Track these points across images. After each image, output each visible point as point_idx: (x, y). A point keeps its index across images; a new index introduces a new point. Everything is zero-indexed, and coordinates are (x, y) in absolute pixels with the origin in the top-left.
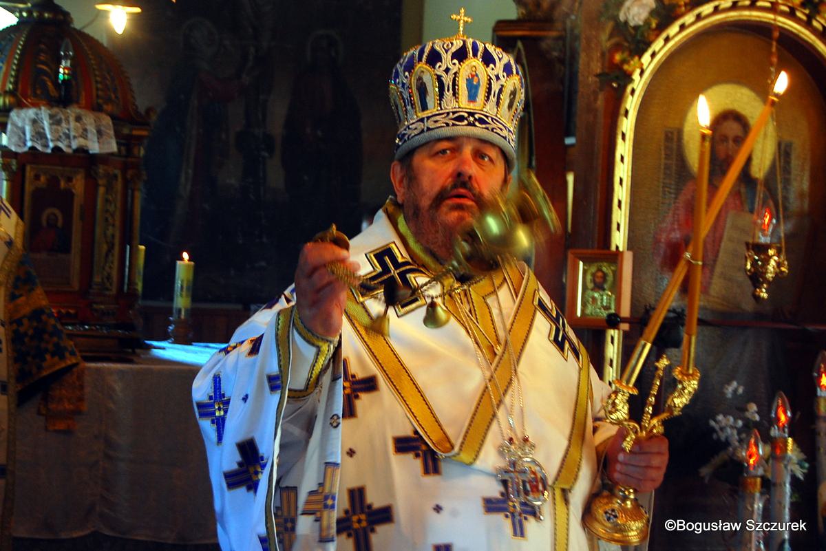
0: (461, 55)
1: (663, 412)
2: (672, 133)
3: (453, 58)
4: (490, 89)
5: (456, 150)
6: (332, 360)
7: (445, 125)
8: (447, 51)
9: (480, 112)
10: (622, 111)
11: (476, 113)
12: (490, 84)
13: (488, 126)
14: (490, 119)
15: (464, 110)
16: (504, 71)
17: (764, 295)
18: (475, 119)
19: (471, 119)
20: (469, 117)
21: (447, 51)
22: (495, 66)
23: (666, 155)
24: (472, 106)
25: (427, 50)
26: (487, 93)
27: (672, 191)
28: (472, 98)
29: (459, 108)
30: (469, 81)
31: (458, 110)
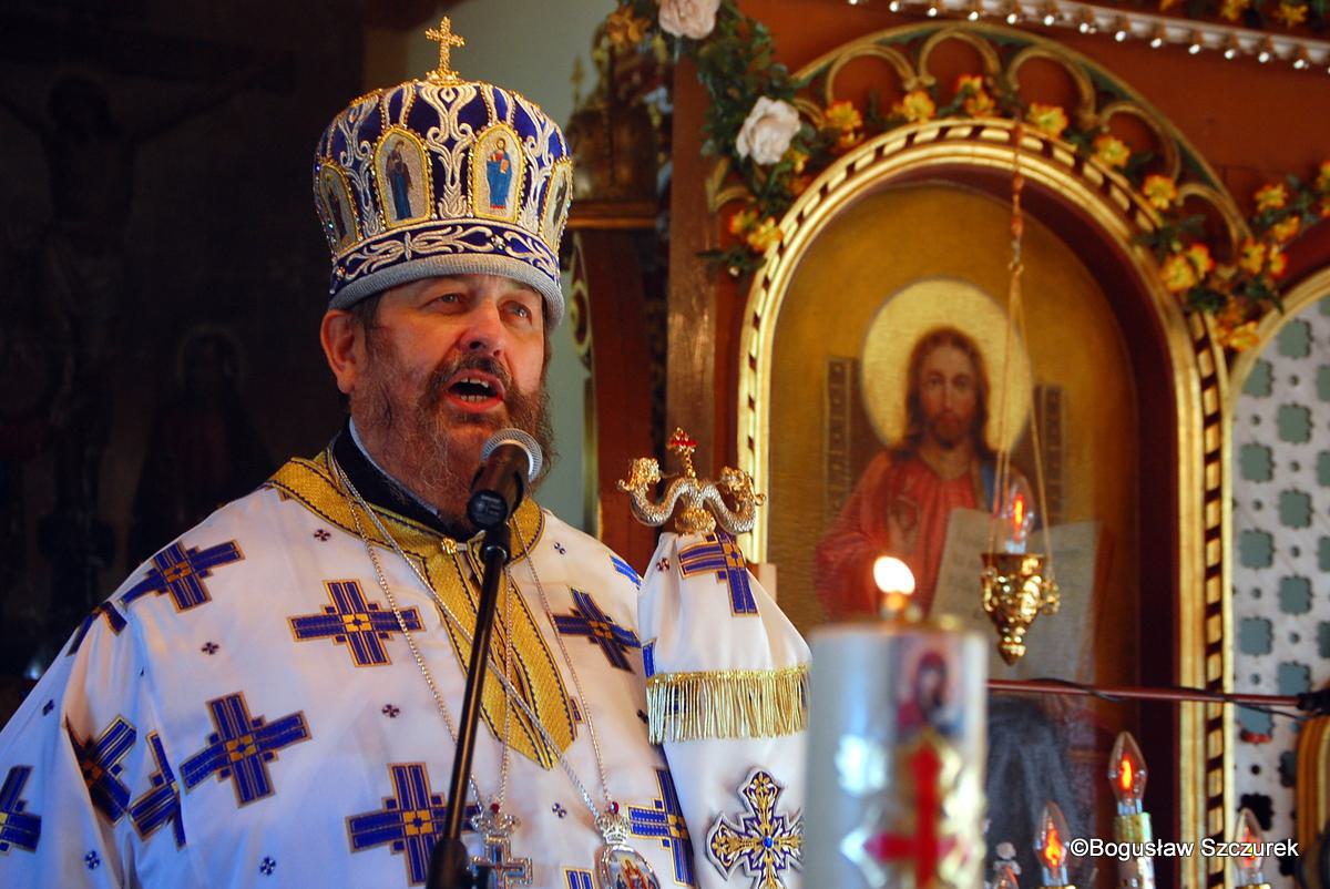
0: (475, 115)
2: (842, 365)
3: (460, 120)
4: (528, 183)
5: (465, 303)
7: (450, 250)
8: (448, 106)
9: (513, 227)
10: (749, 317)
11: (507, 230)
12: (528, 175)
13: (527, 255)
14: (529, 241)
15: (482, 222)
17: (1019, 650)
18: (505, 241)
19: (499, 240)
22: (536, 141)
23: (833, 405)
24: (497, 214)
26: (524, 190)
28: (498, 199)
29: (474, 217)
30: (493, 167)
31: (474, 221)
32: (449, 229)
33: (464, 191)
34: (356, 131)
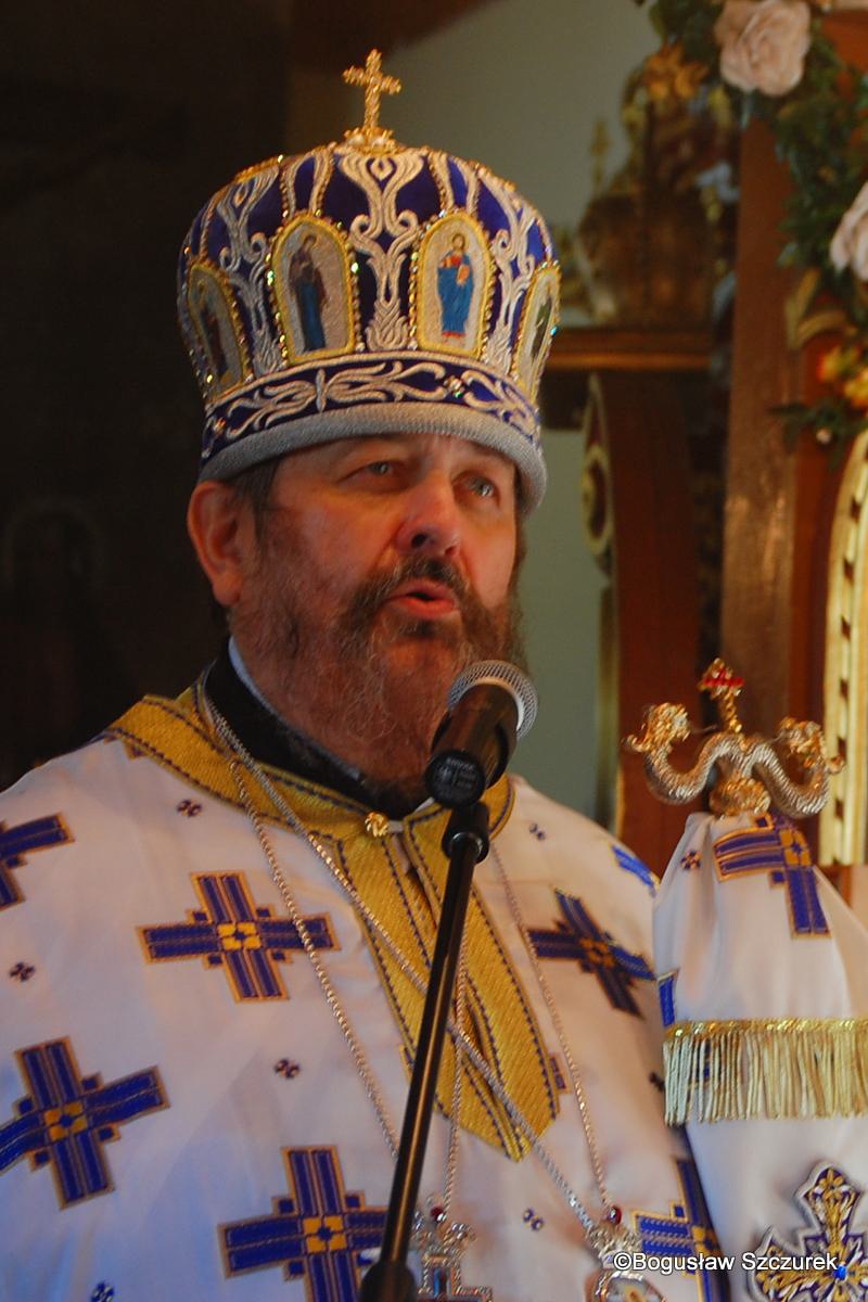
1: (296, 1223)
4: (497, 299)
6: (542, 1124)
7: (381, 396)
8: (382, 184)
12: (498, 286)
13: (495, 405)
14: (498, 384)
15: (431, 356)
16: (528, 253)
19: (455, 384)
20: (447, 377)
21: (382, 184)
24: (452, 344)
25: (322, 177)
27: (465, 435)
28: (454, 323)
29: (419, 349)
32: (382, 366)
33: (404, 309)
34: (244, 220)
